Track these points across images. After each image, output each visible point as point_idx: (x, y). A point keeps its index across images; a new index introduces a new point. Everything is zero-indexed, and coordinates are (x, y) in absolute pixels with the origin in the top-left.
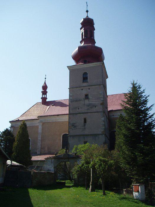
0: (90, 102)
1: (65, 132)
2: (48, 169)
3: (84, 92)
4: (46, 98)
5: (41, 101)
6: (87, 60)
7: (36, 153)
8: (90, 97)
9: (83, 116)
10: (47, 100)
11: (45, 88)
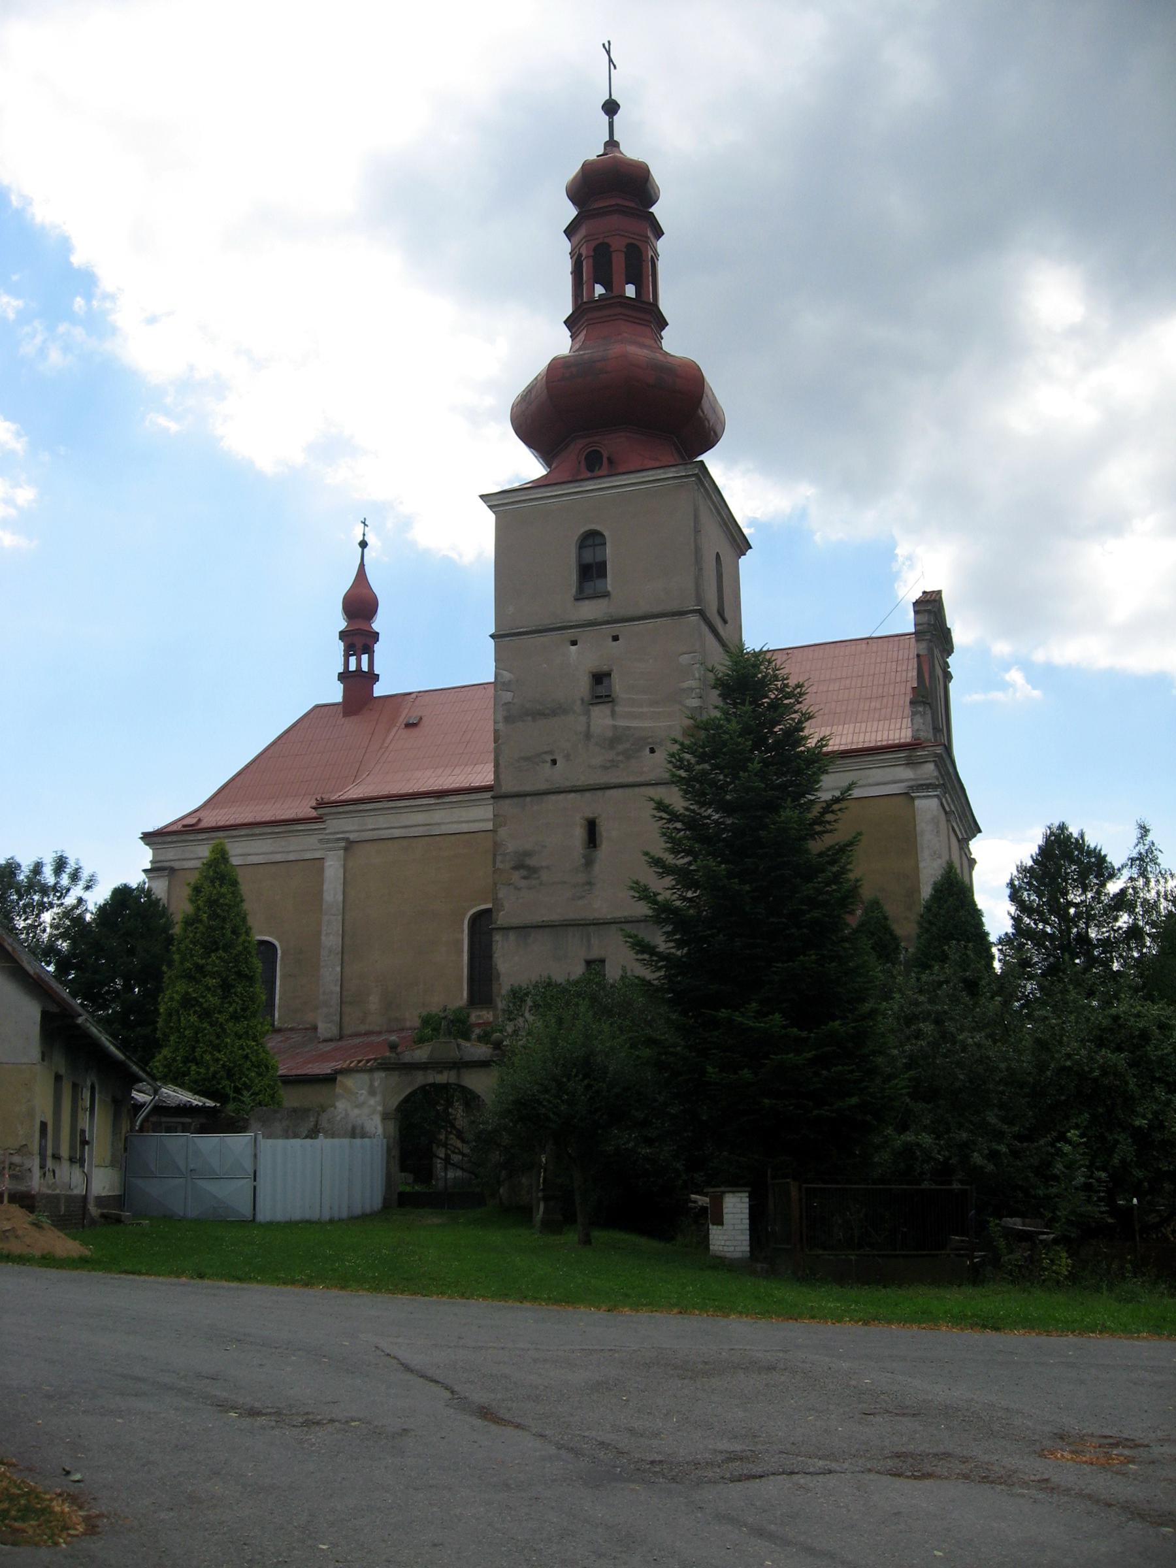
0: (622, 723)
1: (463, 921)
2: (354, 1128)
3: (582, 659)
4: (373, 677)
5: (335, 693)
6: (605, 455)
7: (315, 1028)
8: (618, 685)
9: (586, 806)
10: (379, 690)
11: (360, 607)
